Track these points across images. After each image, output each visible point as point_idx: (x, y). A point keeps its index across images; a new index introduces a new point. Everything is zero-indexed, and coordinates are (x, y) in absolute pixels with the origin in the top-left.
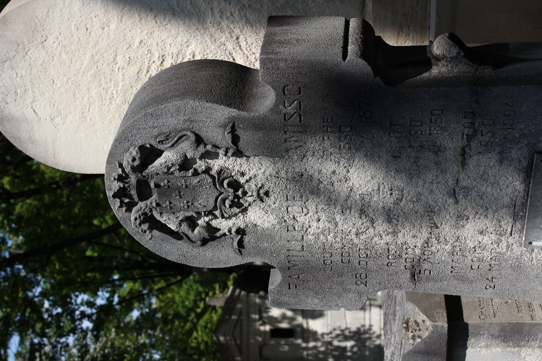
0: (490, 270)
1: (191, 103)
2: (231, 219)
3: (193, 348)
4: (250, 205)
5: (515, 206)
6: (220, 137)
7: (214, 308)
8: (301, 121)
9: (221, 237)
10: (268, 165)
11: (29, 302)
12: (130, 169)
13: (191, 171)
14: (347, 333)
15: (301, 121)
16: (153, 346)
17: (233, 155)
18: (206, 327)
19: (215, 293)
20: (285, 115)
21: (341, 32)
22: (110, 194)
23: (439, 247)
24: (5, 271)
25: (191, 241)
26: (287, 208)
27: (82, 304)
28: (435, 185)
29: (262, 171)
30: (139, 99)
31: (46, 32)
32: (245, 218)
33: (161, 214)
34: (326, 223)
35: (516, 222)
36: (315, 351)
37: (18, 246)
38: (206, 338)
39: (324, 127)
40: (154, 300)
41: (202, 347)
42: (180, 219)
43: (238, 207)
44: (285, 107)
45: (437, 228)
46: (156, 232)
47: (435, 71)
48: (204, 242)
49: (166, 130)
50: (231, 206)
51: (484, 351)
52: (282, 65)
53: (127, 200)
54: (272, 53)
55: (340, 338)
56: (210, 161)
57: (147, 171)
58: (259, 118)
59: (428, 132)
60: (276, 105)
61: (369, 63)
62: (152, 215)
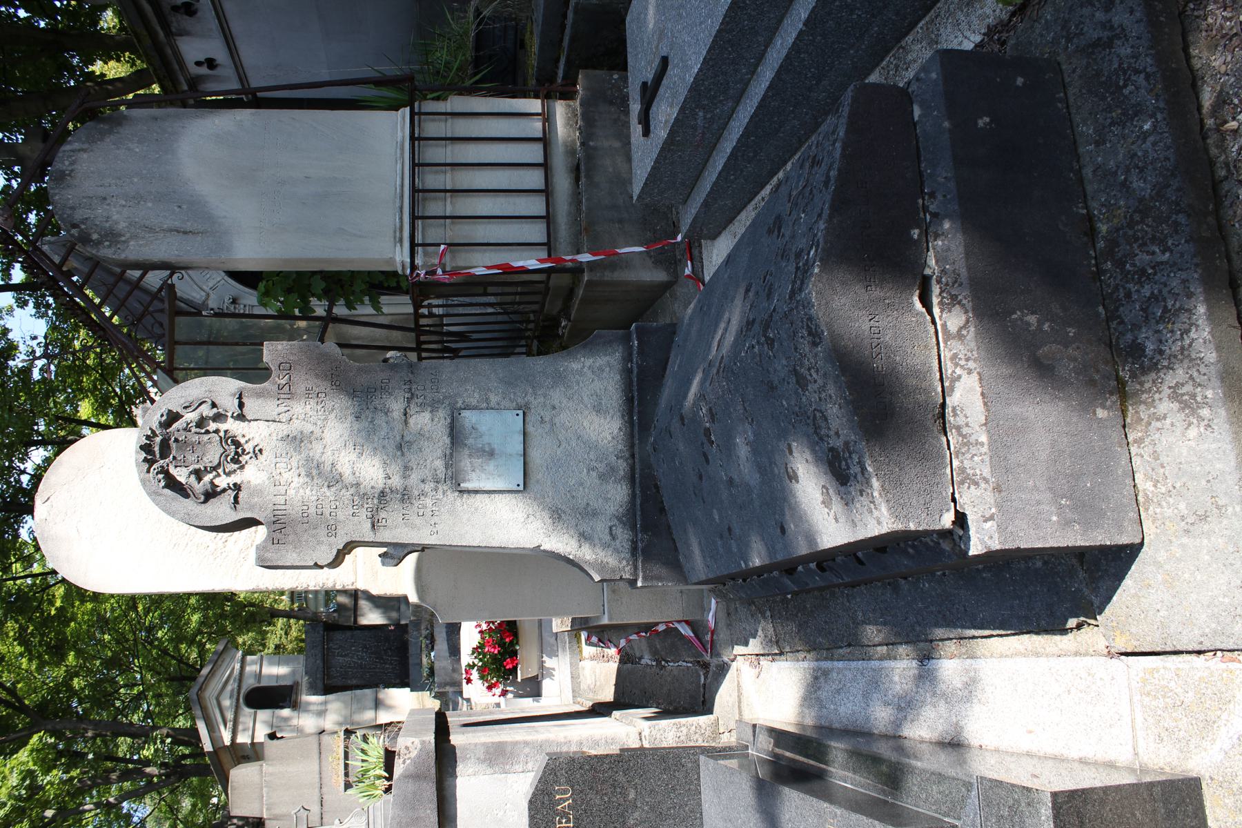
6: (230, 404)
49: (191, 399)
56: (220, 425)
62: (168, 469)
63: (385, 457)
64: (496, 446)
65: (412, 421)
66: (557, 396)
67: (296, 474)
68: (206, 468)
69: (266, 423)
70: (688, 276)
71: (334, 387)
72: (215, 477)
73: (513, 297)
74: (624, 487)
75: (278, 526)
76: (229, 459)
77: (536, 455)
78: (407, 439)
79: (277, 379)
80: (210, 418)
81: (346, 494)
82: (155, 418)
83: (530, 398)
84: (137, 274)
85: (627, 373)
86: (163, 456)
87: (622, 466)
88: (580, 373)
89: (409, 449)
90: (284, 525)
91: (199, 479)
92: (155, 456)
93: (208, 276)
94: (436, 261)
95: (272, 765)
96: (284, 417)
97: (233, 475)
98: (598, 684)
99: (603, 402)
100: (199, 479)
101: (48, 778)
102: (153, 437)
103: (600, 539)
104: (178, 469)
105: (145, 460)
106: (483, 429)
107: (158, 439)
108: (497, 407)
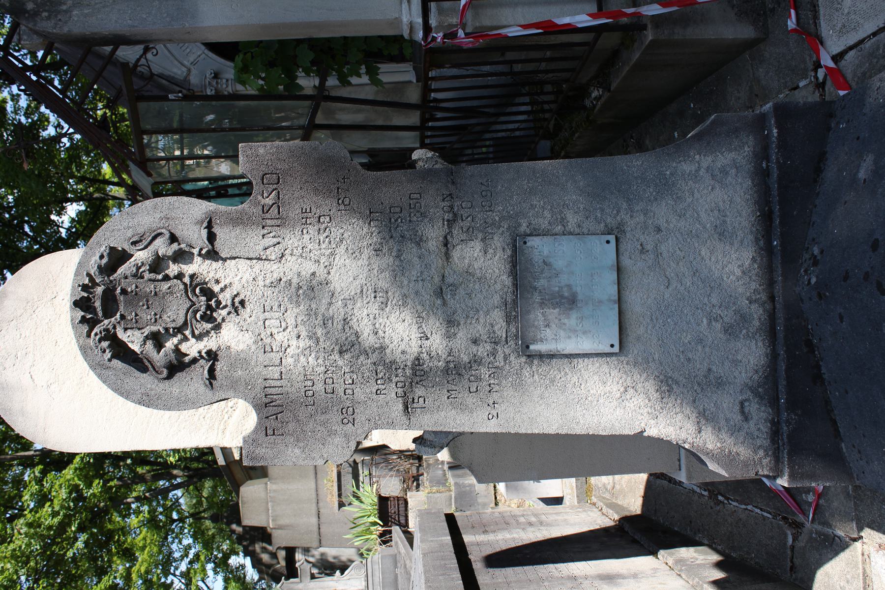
0: (490, 391)
2: (202, 341)
5: (506, 304)
6: (196, 236)
8: (279, 213)
12: (96, 268)
15: (279, 213)
20: (263, 207)
26: (264, 322)
29: (239, 277)
31: (57, 288)
32: (218, 338)
35: (509, 324)
39: (303, 218)
42: (145, 335)
44: (263, 197)
45: (427, 339)
49: (141, 230)
56: (183, 266)
59: (408, 219)
62: (115, 333)
63: (419, 308)
64: (579, 289)
65: (456, 254)
66: (662, 212)
67: (294, 335)
68: (167, 329)
69: (248, 262)
70: (793, 30)
71: (342, 207)
72: (180, 342)
73: (538, 64)
74: (760, 344)
75: (272, 410)
76: (198, 316)
77: (636, 301)
78: (450, 280)
79: (260, 198)
80: (169, 258)
81: (366, 363)
82: (93, 262)
83: (623, 216)
84: (109, 49)
85: (761, 176)
86: (108, 314)
87: (757, 313)
88: (695, 176)
89: (453, 295)
90: (280, 409)
91: (159, 346)
92: (96, 314)
93: (188, 50)
94: (455, 20)
96: (273, 253)
97: (206, 339)
98: (618, 487)
99: (728, 220)
100: (159, 346)
101: (91, 491)
102: (93, 287)
103: (727, 420)
104: (129, 332)
105: (83, 320)
106: (559, 263)
107: (99, 290)
108: (577, 230)
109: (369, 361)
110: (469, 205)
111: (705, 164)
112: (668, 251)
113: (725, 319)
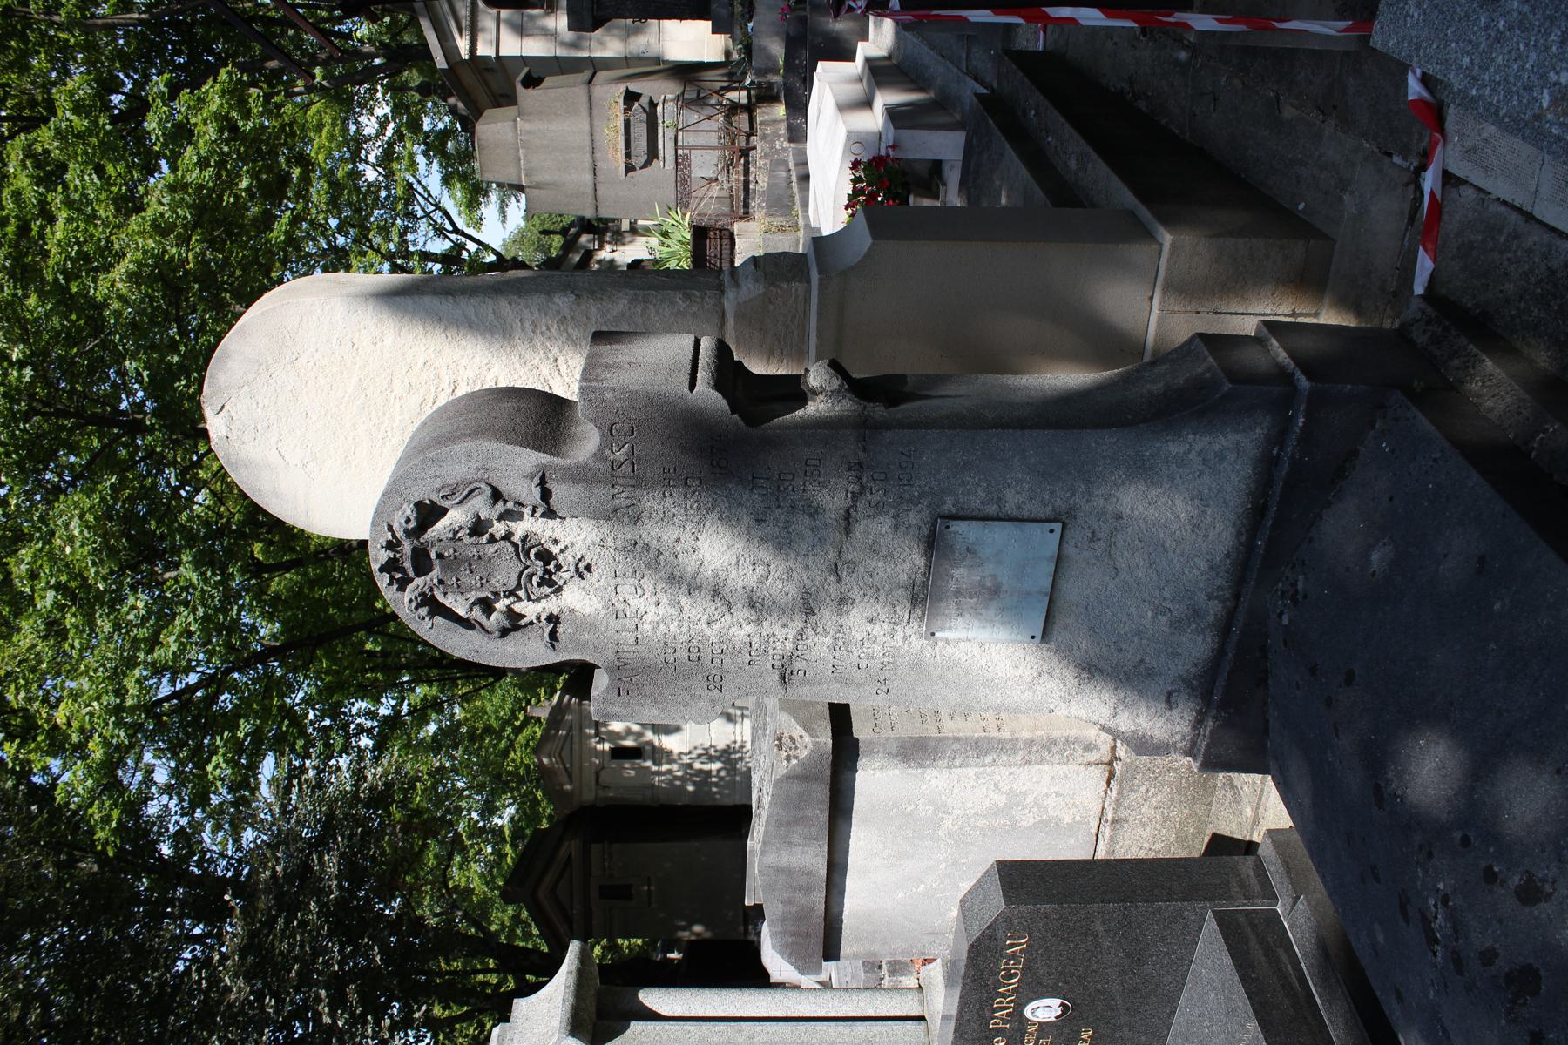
1: (487, 446)
3: (509, 773)
4: (565, 583)
6: (525, 492)
7: (538, 719)
9: (526, 626)
10: (590, 529)
11: (287, 712)
13: (486, 536)
14: (712, 752)
16: (454, 770)
17: (543, 516)
18: (527, 745)
19: (539, 701)
21: (690, 356)
22: (375, 567)
23: (816, 640)
24: (255, 669)
25: (487, 631)
27: (358, 715)
28: (811, 558)
30: (416, 439)
33: (445, 594)
34: (668, 608)
36: (669, 777)
37: (274, 636)
38: (526, 761)
40: (457, 710)
41: (522, 771)
43: (550, 586)
45: (814, 614)
46: (438, 619)
47: (813, 408)
48: (504, 633)
49: (452, 481)
50: (540, 585)
51: (878, 774)
52: (609, 395)
53: (398, 576)
54: (596, 380)
55: (703, 759)
56: (511, 524)
57: (426, 536)
58: (577, 466)
60: (601, 450)
61: (724, 397)
62: (433, 595)
74: (1209, 639)
85: (1267, 465)
87: (1214, 609)
95: (529, 121)
109: (743, 633)
110: (883, 477)
111: (1198, 446)
112: (1125, 541)
113: (1175, 613)
